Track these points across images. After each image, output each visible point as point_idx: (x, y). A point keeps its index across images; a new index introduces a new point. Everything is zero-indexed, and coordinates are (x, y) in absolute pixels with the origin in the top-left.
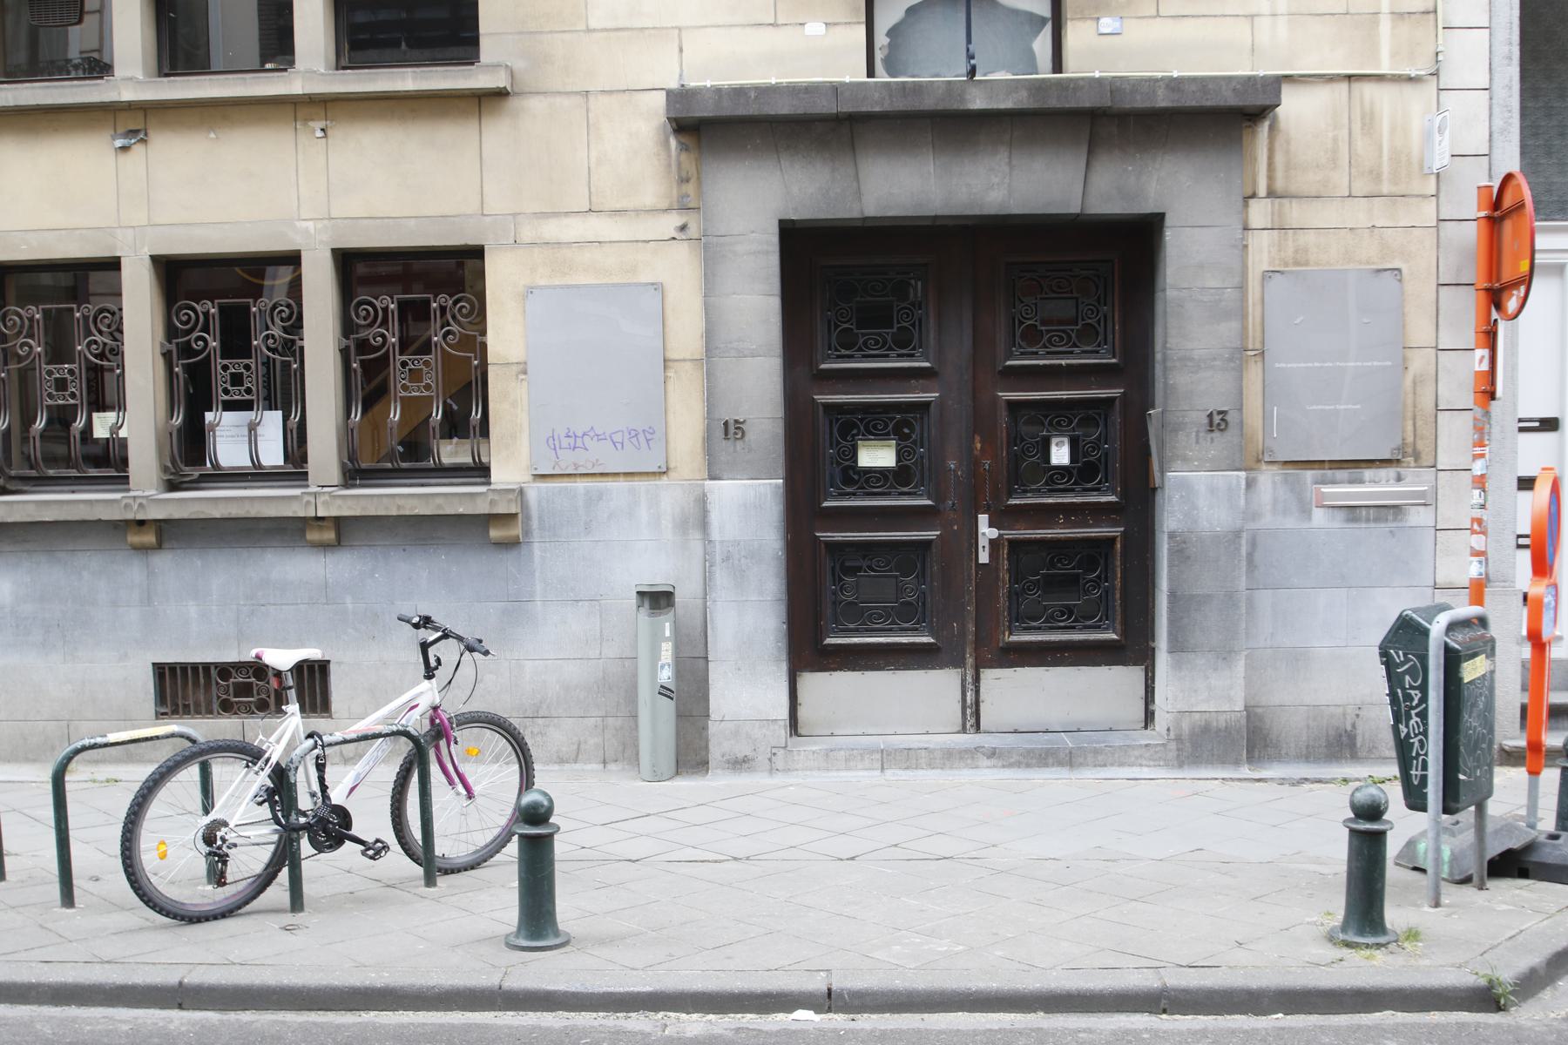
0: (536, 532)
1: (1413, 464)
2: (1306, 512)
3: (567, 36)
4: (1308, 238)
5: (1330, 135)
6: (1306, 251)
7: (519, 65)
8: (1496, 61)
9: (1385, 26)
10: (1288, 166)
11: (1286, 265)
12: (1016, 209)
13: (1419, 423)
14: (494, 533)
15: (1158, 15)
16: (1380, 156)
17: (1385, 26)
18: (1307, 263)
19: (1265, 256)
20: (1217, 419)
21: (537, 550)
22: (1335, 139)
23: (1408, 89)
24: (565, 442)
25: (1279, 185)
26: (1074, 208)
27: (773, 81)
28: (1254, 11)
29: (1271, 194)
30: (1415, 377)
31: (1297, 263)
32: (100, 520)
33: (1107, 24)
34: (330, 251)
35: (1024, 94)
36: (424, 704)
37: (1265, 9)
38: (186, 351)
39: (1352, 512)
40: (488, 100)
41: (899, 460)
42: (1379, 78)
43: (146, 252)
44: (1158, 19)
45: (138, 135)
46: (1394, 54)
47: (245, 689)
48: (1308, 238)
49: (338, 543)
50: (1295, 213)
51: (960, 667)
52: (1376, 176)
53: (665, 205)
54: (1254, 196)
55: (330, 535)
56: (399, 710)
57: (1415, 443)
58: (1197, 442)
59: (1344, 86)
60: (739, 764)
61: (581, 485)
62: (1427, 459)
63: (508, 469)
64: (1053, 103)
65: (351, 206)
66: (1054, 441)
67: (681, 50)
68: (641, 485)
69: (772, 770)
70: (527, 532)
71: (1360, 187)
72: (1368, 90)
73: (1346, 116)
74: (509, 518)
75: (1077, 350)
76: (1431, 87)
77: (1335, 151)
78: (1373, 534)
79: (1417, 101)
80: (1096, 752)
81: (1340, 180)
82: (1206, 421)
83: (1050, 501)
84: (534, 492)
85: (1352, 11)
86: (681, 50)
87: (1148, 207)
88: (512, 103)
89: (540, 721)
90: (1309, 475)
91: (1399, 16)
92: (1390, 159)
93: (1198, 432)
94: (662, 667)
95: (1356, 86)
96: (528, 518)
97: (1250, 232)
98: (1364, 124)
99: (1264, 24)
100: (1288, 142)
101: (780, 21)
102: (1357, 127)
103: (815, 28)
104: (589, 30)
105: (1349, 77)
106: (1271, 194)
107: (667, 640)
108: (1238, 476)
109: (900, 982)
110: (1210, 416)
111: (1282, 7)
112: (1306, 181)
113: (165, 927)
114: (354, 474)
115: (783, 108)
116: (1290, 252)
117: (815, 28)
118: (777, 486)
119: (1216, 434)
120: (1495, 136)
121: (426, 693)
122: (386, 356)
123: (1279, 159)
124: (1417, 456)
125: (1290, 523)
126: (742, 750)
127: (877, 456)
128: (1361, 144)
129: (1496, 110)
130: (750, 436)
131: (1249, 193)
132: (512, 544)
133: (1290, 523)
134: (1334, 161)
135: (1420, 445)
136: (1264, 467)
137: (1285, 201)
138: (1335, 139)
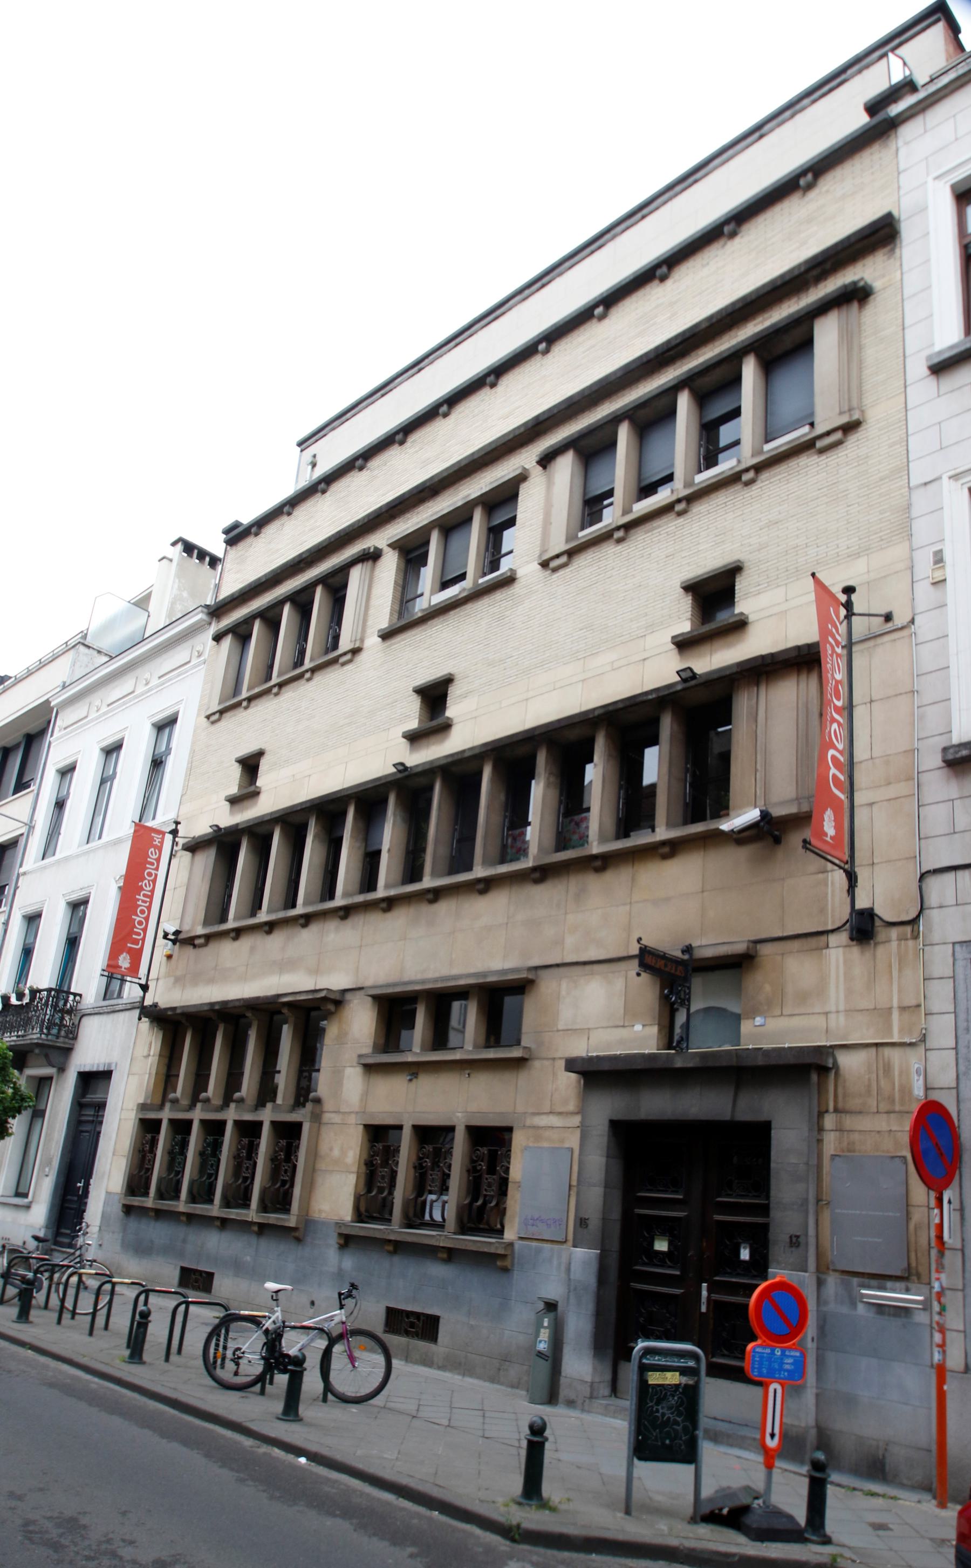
0: (516, 1266)
1: (916, 1281)
2: (853, 1305)
3: (550, 1033)
4: (856, 1137)
5: (867, 1077)
6: (854, 1143)
7: (533, 1046)
8: (959, 1033)
9: (895, 1015)
10: (845, 1096)
11: (843, 1151)
12: (703, 1117)
13: (919, 1255)
14: (499, 1263)
15: (782, 1015)
16: (894, 1089)
17: (895, 1015)
18: (854, 1151)
19: (832, 1145)
20: (794, 1239)
21: (515, 1272)
22: (869, 1080)
23: (909, 1051)
24: (531, 1221)
25: (840, 1105)
26: (727, 1117)
27: (618, 1053)
28: (827, 1010)
29: (836, 1110)
30: (916, 1225)
31: (849, 1151)
32: (376, 1238)
33: (759, 1020)
34: (606, 1123)
35: (698, 1059)
36: (337, 1319)
37: (833, 1009)
38: (474, 1168)
39: (880, 1309)
40: (519, 1063)
41: (669, 1248)
42: (893, 1045)
43: (411, 1123)
44: (782, 1017)
45: (415, 1075)
46: (901, 1031)
47: (412, 1325)
48: (856, 1137)
49: (395, 1252)
50: (849, 1122)
51: (695, 1376)
52: (891, 1100)
53: (576, 1111)
54: (827, 1111)
55: (391, 1248)
56: (325, 1320)
57: (917, 1267)
58: (784, 1252)
59: (873, 1050)
60: (571, 1403)
61: (534, 1244)
62: (925, 1279)
63: (510, 1235)
64: (710, 1064)
65: (473, 1107)
66: (742, 1246)
67: (588, 1039)
68: (556, 1247)
69: (583, 1410)
70: (513, 1265)
71: (883, 1107)
72: (887, 1051)
73: (875, 1066)
74: (504, 1257)
75: (751, 1195)
76: (921, 1049)
77: (869, 1086)
78: (894, 1324)
79: (914, 1059)
80: (729, 1436)
81: (873, 1103)
82: (788, 1240)
83: (734, 1280)
84: (518, 1245)
85: (878, 1007)
86: (588, 1039)
87: (763, 1117)
88: (530, 1063)
89: (507, 1363)
90: (855, 1281)
91: (903, 1009)
92: (899, 1091)
93: (785, 1246)
94: (540, 1342)
95: (880, 1049)
96: (513, 1258)
97: (846, 1133)
98: (884, 1070)
99: (832, 1017)
100: (845, 1081)
101: (626, 1024)
102: (881, 1072)
103: (638, 1027)
104: (558, 1031)
105: (877, 1045)
106: (836, 1110)
107: (546, 1328)
108: (804, 1276)
109: (338, 1457)
110: (791, 1237)
111: (842, 1008)
112: (854, 1103)
113: (215, 1388)
114: (227, 1203)
115: (606, 1067)
116: (845, 1144)
117: (638, 1027)
118: (597, 1253)
119: (793, 1249)
120: (961, 1076)
121: (339, 1315)
122: (426, 1171)
123: (840, 1090)
124: (919, 1276)
125: (845, 1310)
126: (572, 1396)
127: (661, 1246)
128: (883, 1083)
129: (961, 1061)
130: (590, 1227)
131: (824, 1110)
132: (506, 1270)
133: (845, 1310)
134: (869, 1091)
135: (921, 1269)
136: (831, 1273)
137: (843, 1115)
138: (869, 1080)
